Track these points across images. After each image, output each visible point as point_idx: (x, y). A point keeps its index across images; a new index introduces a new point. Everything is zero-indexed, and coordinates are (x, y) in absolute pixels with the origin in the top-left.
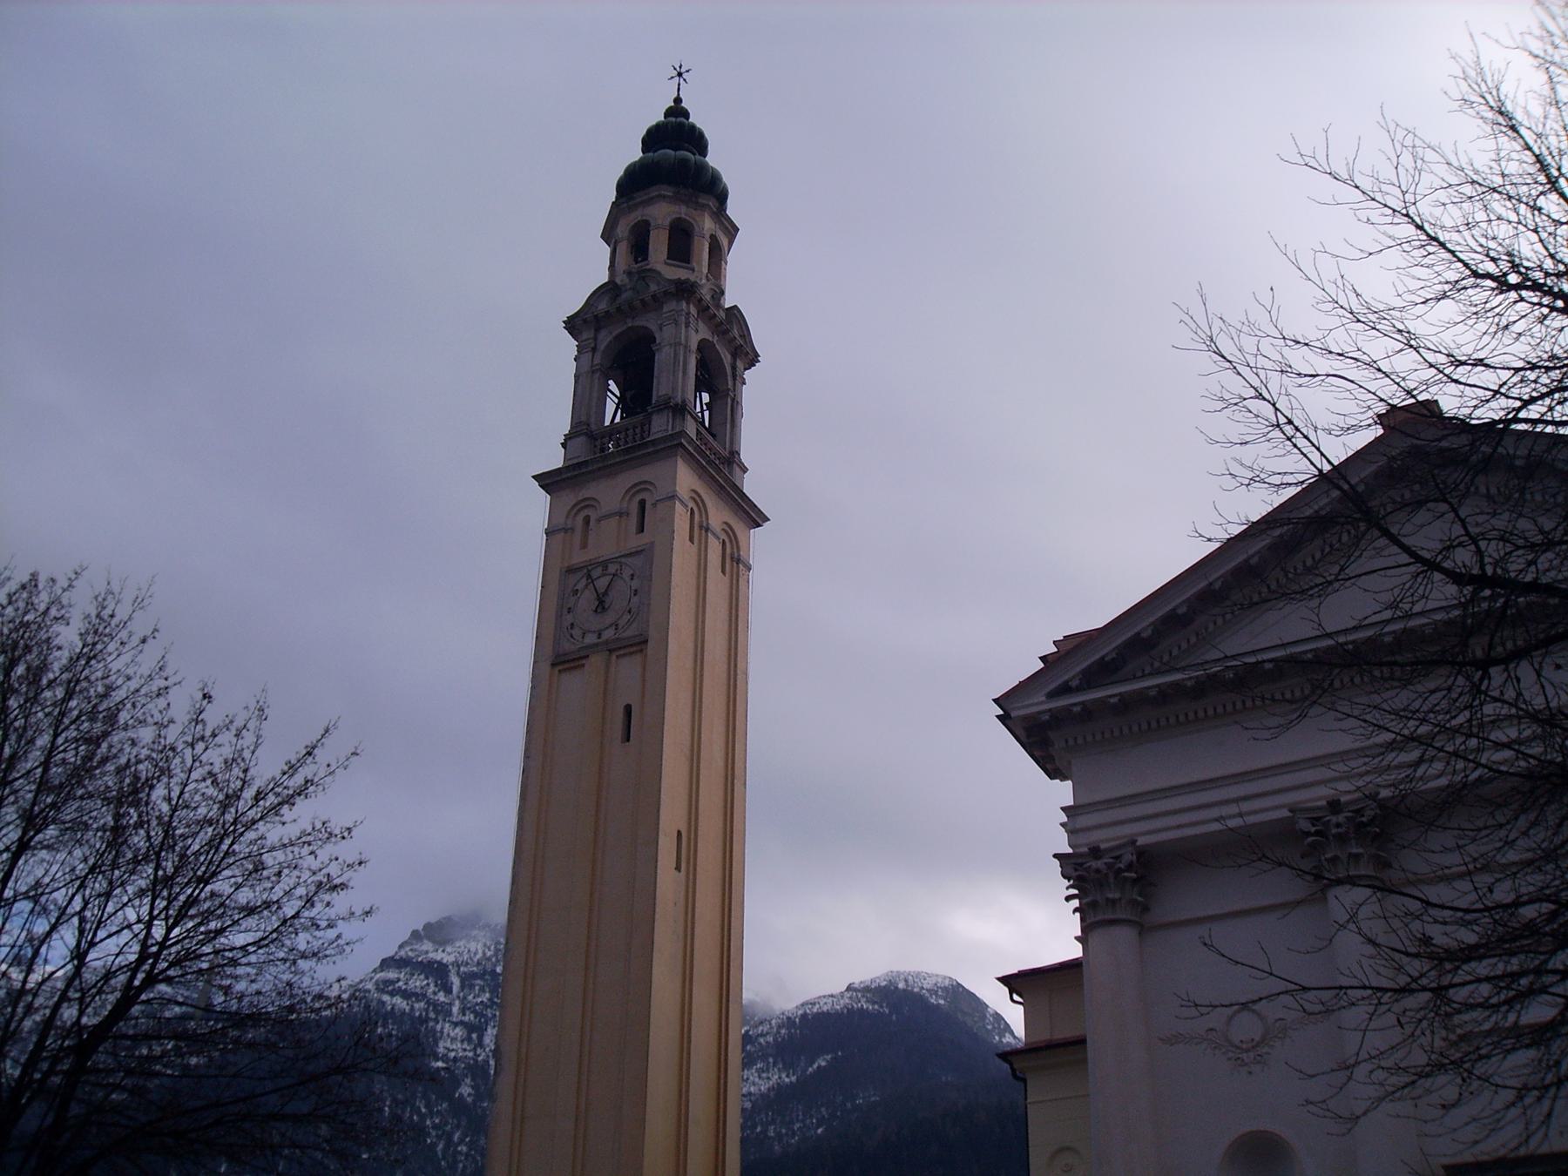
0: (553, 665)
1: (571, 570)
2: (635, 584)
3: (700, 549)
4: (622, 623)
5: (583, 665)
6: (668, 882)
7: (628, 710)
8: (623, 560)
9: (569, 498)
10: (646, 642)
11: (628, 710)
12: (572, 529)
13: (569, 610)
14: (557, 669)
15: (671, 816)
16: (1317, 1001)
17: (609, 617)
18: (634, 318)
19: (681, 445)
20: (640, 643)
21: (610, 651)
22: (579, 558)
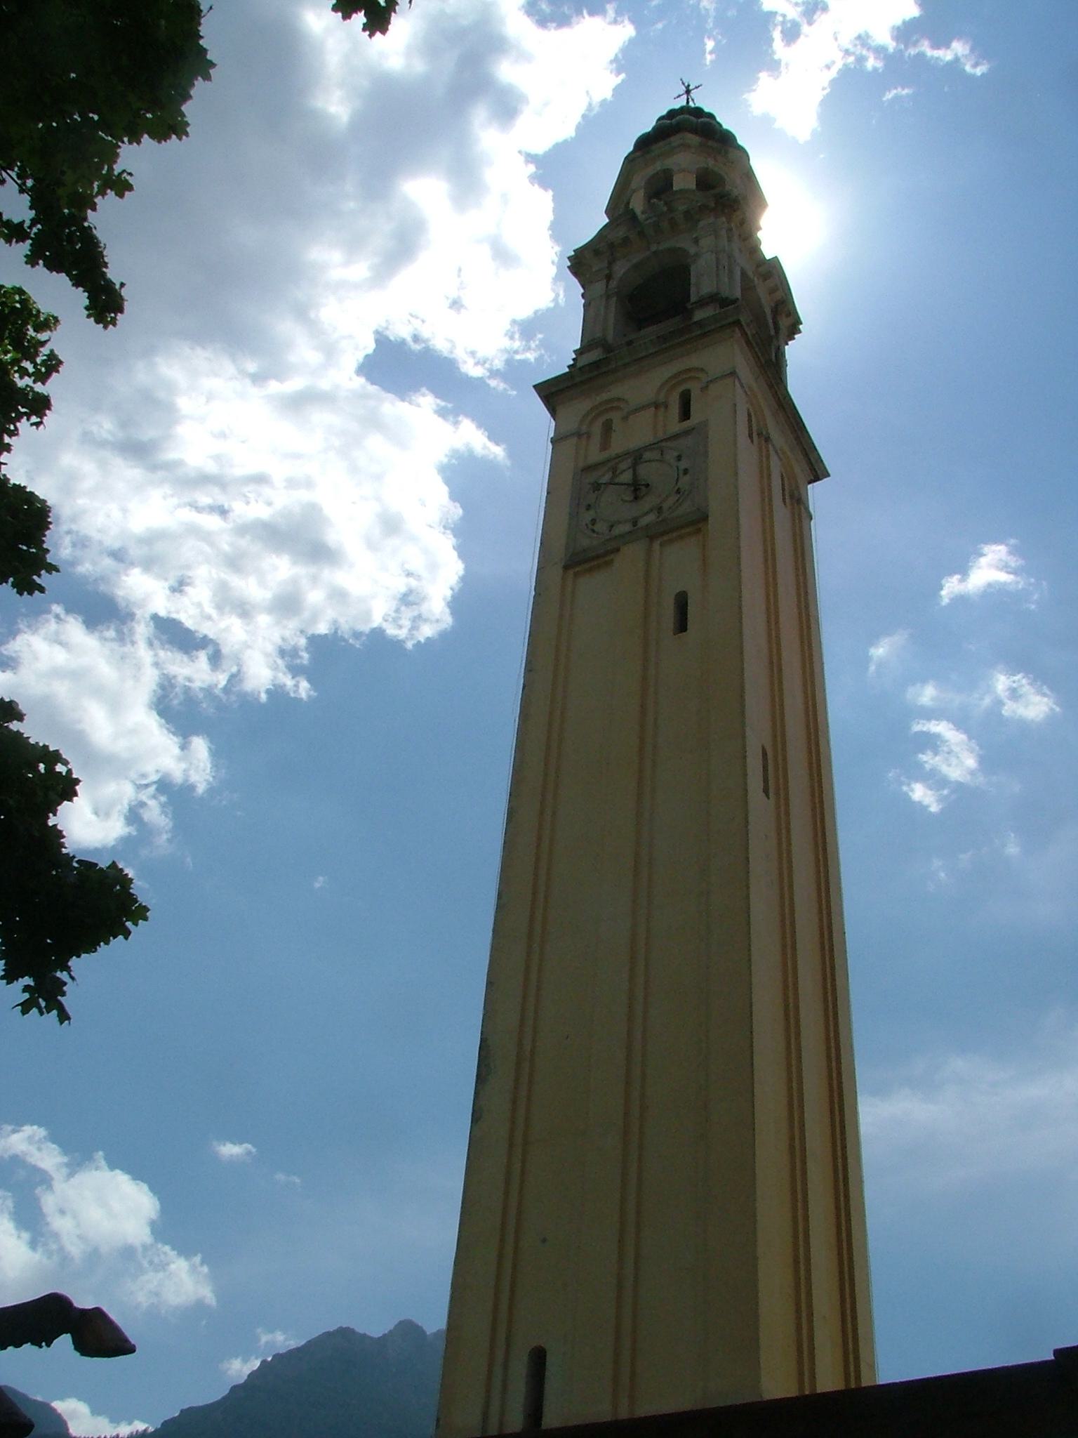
0: (566, 568)
1: (588, 469)
2: (683, 464)
3: (778, 807)
4: (665, 506)
5: (612, 561)
6: (760, 807)
7: (539, 1358)
8: (664, 444)
9: (578, 408)
10: (705, 518)
11: (539, 1358)
12: (589, 436)
13: (589, 507)
14: (571, 572)
15: (757, 735)
16: (686, 84)
17: (649, 502)
18: (659, 243)
19: (737, 323)
20: (698, 521)
21: (652, 538)
22: (595, 455)
